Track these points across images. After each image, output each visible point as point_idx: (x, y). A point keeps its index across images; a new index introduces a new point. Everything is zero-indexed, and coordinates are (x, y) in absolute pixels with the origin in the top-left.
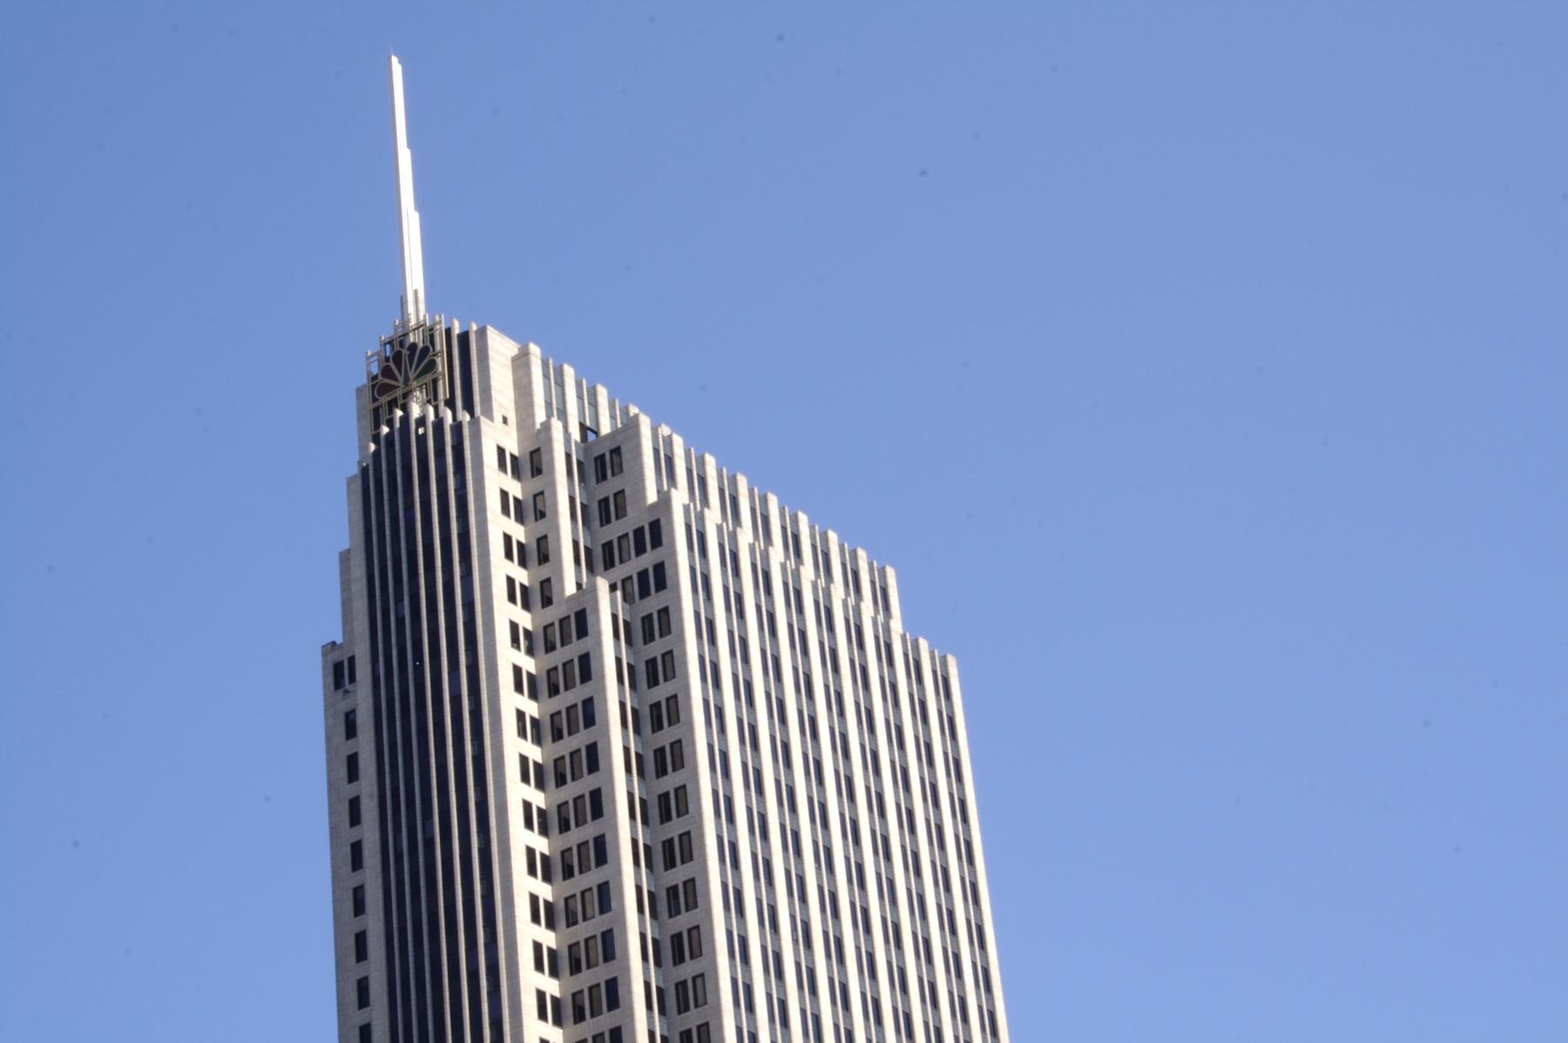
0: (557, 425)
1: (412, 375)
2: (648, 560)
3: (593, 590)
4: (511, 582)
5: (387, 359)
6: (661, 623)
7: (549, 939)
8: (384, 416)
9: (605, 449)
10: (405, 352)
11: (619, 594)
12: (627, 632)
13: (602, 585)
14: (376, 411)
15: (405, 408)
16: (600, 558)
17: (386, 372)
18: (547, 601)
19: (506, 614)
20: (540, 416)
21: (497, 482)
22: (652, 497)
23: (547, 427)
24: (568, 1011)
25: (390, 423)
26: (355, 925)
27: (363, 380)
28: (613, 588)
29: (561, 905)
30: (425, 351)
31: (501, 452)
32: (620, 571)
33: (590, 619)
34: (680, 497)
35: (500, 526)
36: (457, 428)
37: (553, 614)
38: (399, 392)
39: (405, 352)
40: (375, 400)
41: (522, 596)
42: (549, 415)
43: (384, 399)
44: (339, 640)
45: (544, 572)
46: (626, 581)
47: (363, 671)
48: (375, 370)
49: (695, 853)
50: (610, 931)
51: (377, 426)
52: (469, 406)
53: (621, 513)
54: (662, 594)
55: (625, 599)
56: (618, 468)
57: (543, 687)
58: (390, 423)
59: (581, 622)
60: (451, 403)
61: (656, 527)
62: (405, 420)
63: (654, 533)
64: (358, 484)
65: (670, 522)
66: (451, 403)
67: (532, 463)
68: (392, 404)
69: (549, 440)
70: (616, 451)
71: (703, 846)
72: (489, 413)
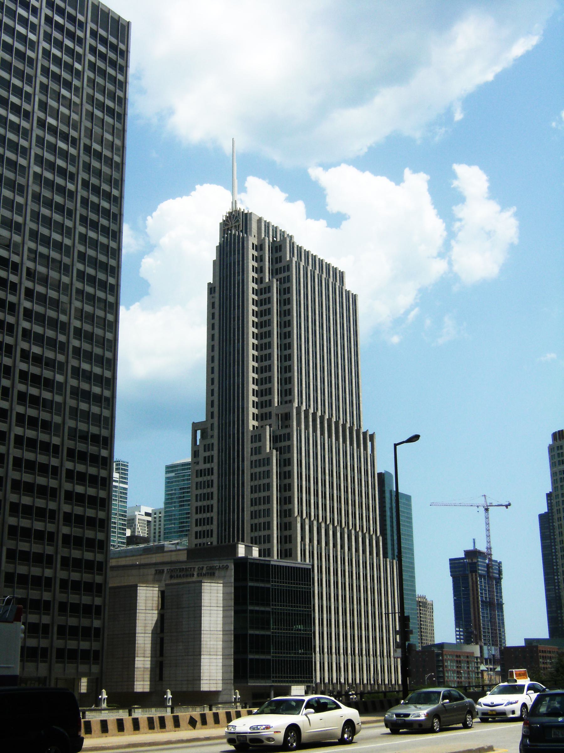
0: (267, 238)
1: (233, 223)
2: (286, 274)
3: (273, 282)
4: (253, 299)
5: (227, 217)
6: (288, 290)
7: (256, 309)
8: (226, 232)
9: (278, 245)
10: (232, 216)
11: (278, 282)
12: (279, 292)
13: (275, 280)
14: (224, 230)
15: (231, 231)
16: (274, 272)
17: (227, 220)
18: (261, 282)
19: (252, 285)
20: (263, 236)
21: (251, 252)
22: (288, 259)
23: (264, 239)
24: (259, 336)
25: (227, 234)
26: (211, 398)
27: (221, 221)
28: (277, 281)
29: (259, 357)
30: (237, 217)
31: (253, 244)
32: (279, 276)
33: (271, 288)
34: (295, 259)
35: (251, 263)
36: (243, 237)
37: (263, 286)
38: (230, 226)
39: (232, 216)
40: (224, 227)
41: (255, 280)
42: (265, 236)
43: (226, 227)
44: (212, 282)
45: (261, 253)
46: (281, 279)
47: (217, 289)
48: (224, 219)
49: (291, 347)
50: (270, 365)
51: (224, 234)
52: (246, 233)
53: (281, 261)
54: (289, 294)
55: (280, 283)
56: (280, 250)
57: (259, 371)
58: (227, 234)
59: (268, 289)
60: (242, 231)
61: (288, 266)
62: (231, 234)
63: (288, 268)
64: (219, 248)
65: (292, 265)
66: (242, 231)
67: (259, 247)
68: (228, 229)
69: (265, 242)
70: (280, 246)
71: (293, 346)
72: (251, 235)
